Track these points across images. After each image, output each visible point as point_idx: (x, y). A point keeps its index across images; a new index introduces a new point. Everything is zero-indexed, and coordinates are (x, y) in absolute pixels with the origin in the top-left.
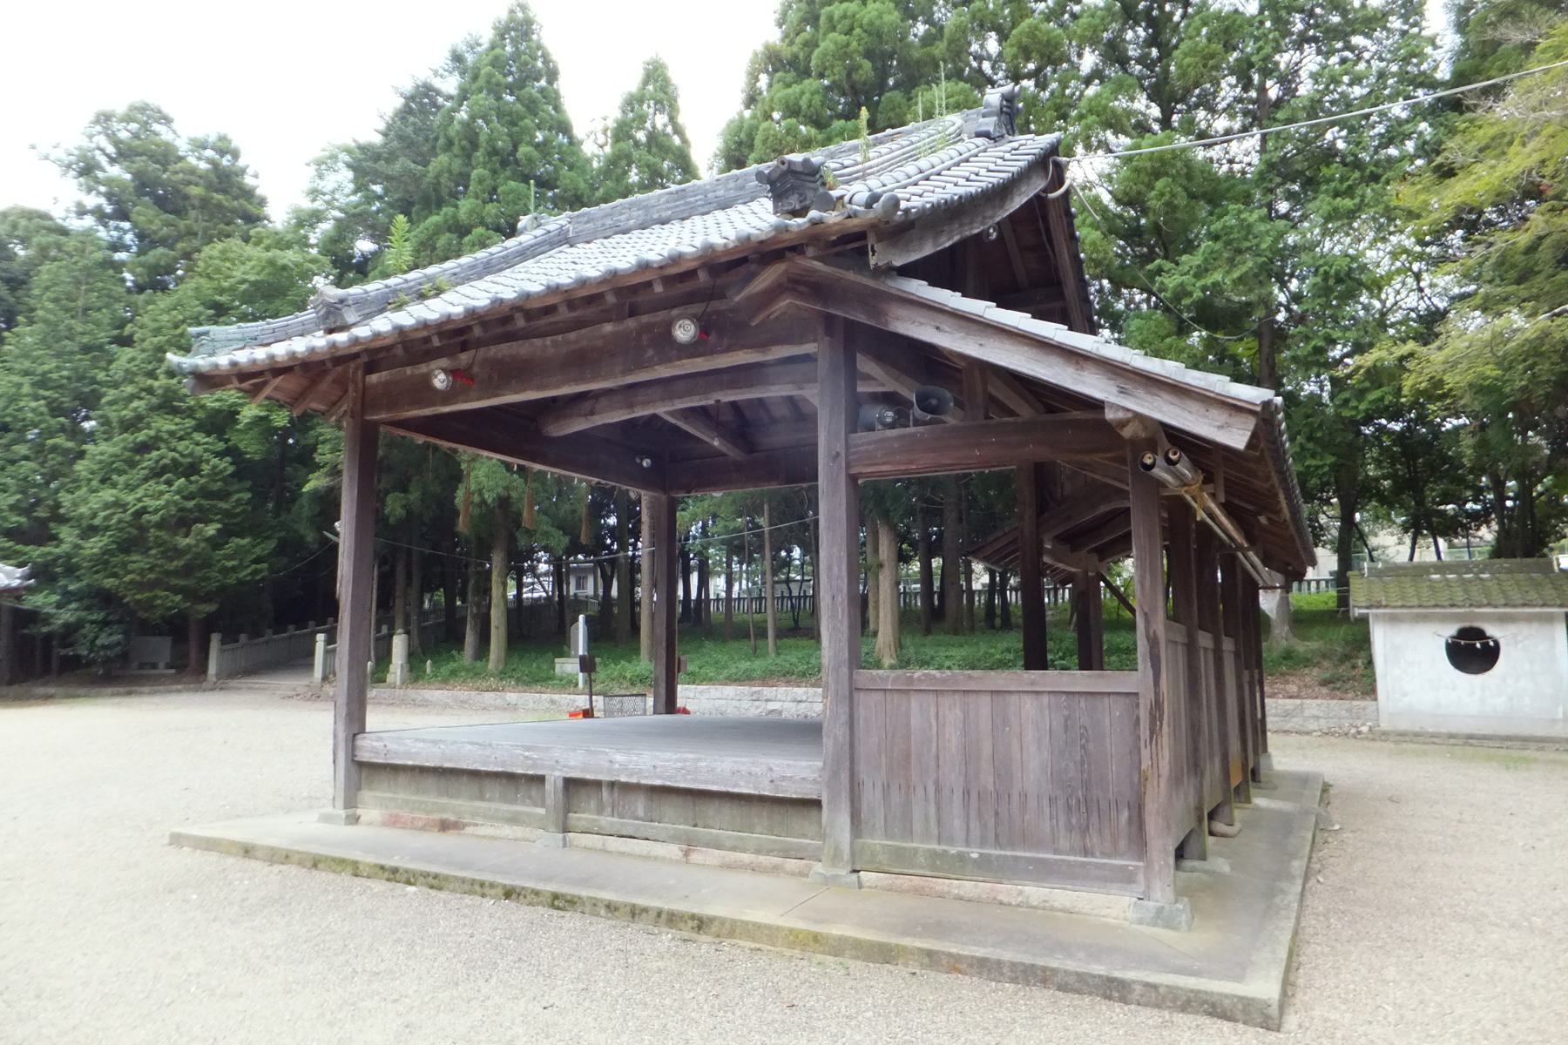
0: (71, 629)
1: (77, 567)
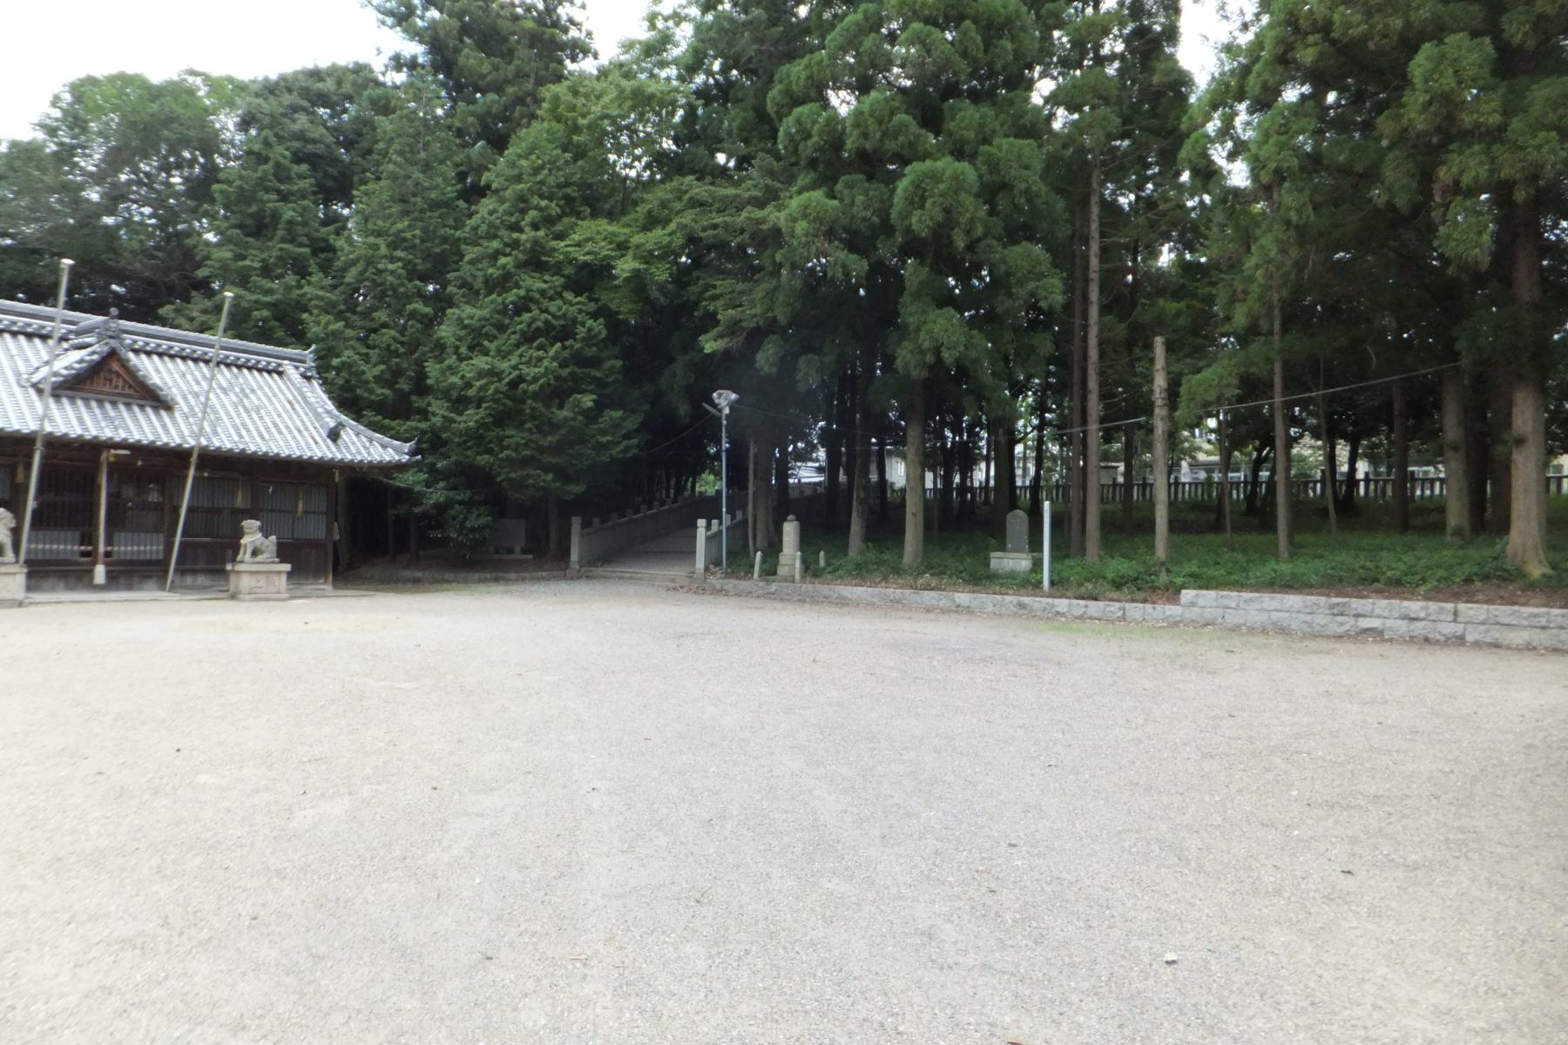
0: (441, 508)
1: (445, 443)
